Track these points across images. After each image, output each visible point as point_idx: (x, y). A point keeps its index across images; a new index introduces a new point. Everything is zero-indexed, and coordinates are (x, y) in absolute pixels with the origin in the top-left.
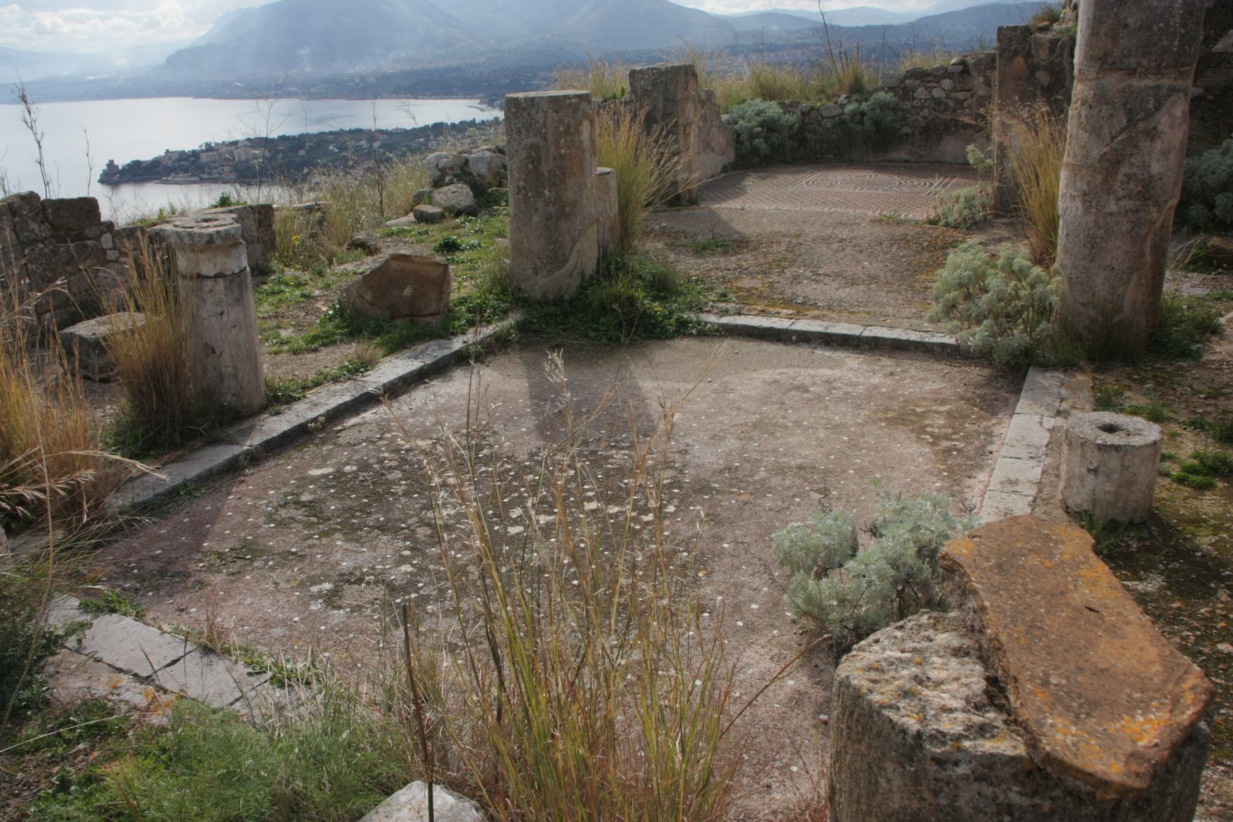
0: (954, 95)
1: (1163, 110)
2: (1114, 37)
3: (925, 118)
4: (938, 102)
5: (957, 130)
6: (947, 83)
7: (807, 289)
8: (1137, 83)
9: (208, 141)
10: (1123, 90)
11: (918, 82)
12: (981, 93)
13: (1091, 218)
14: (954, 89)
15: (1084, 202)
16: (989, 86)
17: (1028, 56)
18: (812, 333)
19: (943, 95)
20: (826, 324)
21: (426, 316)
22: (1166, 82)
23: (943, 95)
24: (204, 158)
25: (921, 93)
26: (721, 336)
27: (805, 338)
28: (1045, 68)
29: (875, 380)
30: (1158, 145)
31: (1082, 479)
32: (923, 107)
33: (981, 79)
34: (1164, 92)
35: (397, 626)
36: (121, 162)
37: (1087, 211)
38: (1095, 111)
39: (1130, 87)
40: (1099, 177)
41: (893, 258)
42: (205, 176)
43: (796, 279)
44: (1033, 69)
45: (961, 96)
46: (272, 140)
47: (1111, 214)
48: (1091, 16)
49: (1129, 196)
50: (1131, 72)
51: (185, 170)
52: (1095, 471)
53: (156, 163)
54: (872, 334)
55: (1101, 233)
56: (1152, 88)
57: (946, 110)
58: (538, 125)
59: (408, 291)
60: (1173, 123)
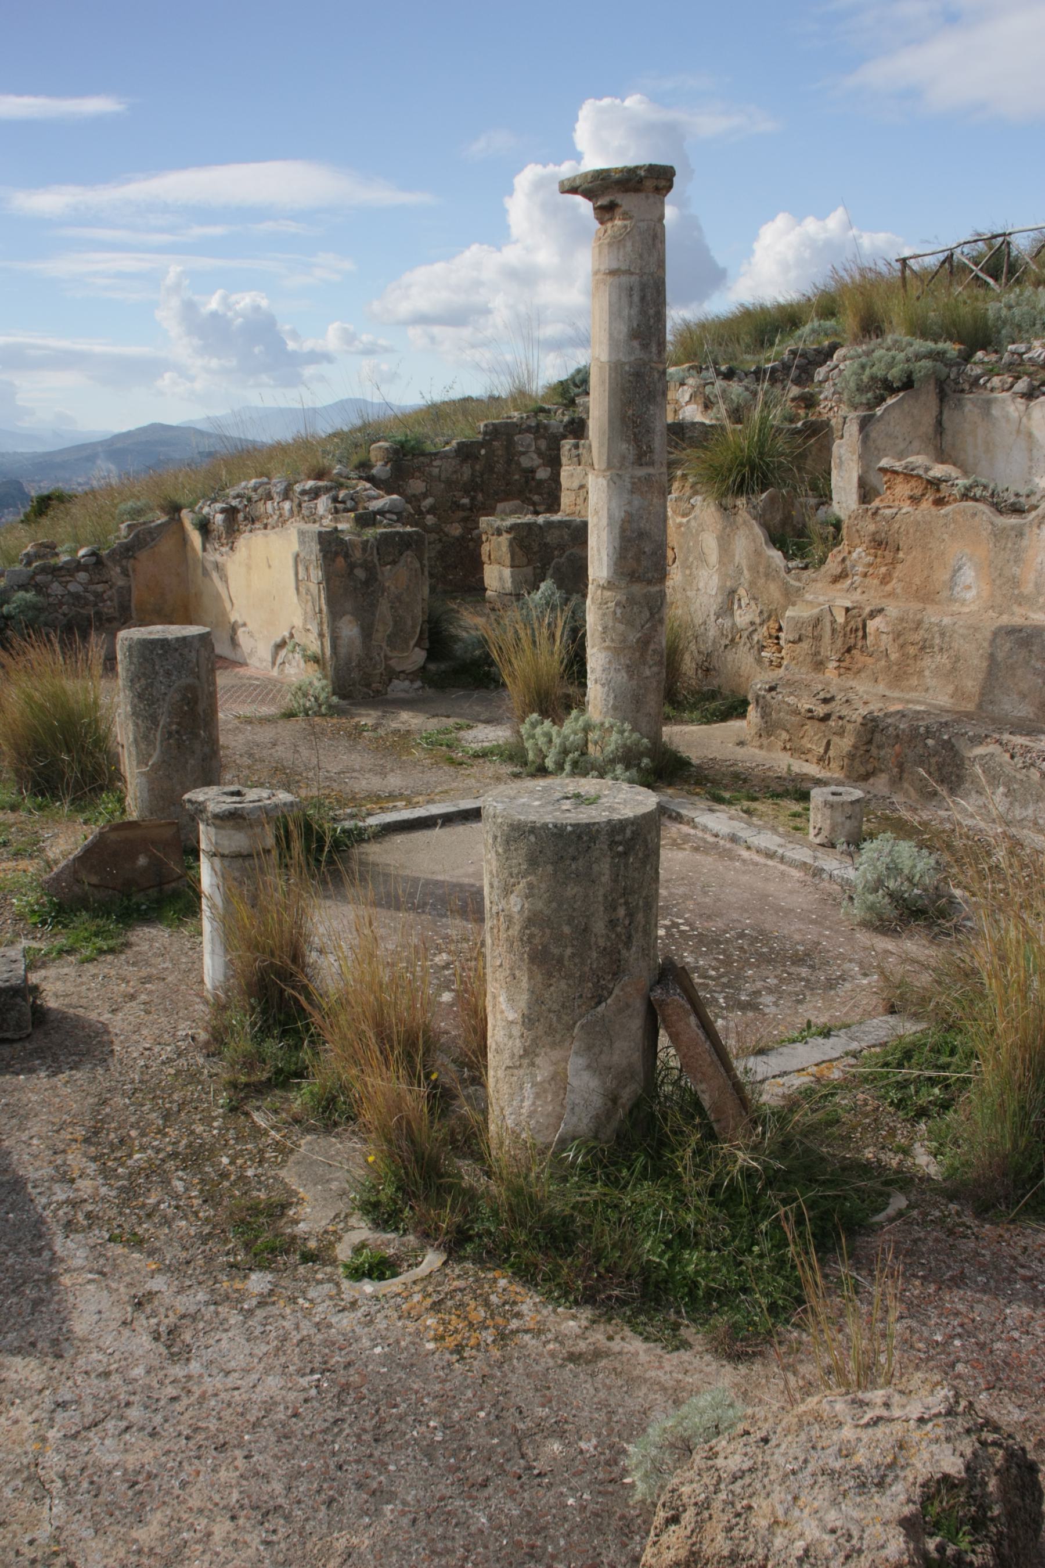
0: (92, 587)
2: (638, 560)
3: (65, 615)
4: (76, 596)
5: (101, 625)
6: (82, 576)
11: (50, 577)
12: (120, 583)
13: (635, 682)
14: (91, 582)
15: (628, 672)
16: (128, 576)
17: (347, 556)
18: (453, 813)
19: (81, 589)
21: (168, 882)
23: (81, 589)
25: (56, 588)
26: (384, 835)
27: (448, 819)
28: (361, 566)
31: (843, 824)
32: (61, 604)
33: (118, 570)
37: (631, 678)
40: (638, 654)
44: (352, 566)
45: (100, 588)
48: (617, 545)
49: (655, 664)
52: (849, 818)
54: (427, 814)
55: (642, 691)
57: (86, 604)
58: (191, 665)
59: (142, 861)
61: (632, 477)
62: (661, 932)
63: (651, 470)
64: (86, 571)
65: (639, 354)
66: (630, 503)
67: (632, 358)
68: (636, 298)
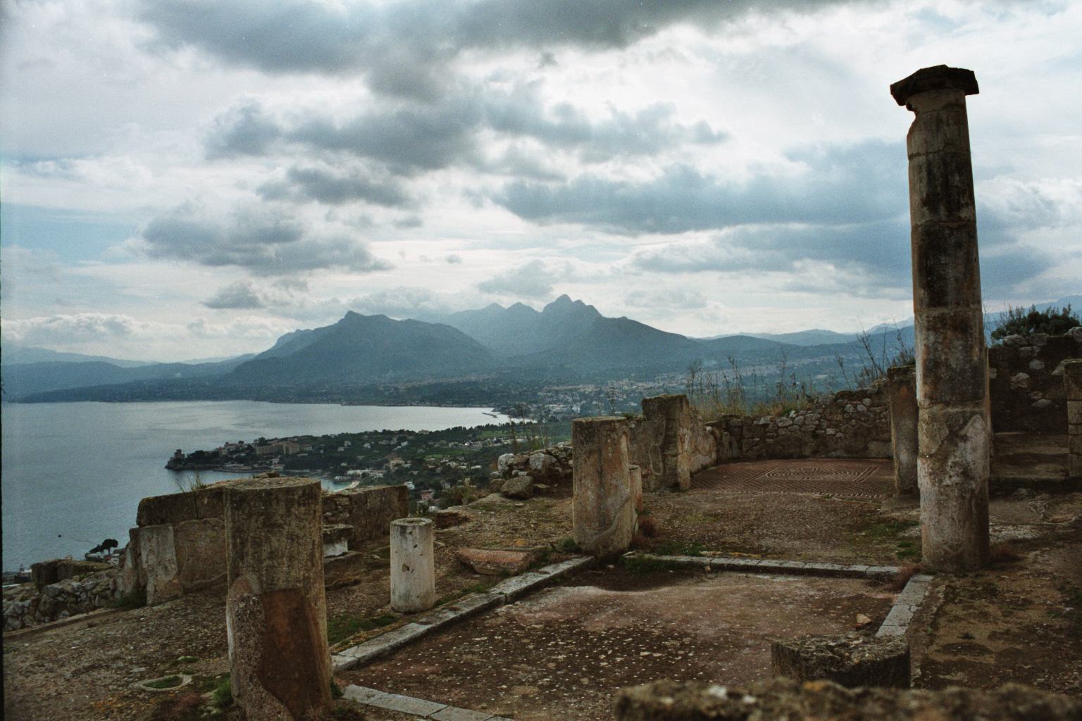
0: (873, 409)
1: (969, 424)
3: (853, 426)
7: (767, 542)
8: (951, 410)
9: (242, 439)
10: (945, 414)
13: (936, 488)
14: (873, 405)
20: (781, 561)
22: (968, 409)
24: (258, 451)
25: (849, 408)
29: (811, 593)
30: (969, 445)
32: (851, 418)
34: (968, 414)
35: (517, 674)
36: (188, 450)
37: (933, 484)
38: (930, 426)
39: (948, 412)
41: (826, 522)
42: (256, 466)
43: (760, 537)
45: (878, 409)
46: (316, 438)
47: (948, 486)
50: (947, 404)
51: (240, 460)
53: (216, 454)
56: (961, 413)
60: (978, 431)
61: (928, 317)
62: (668, 701)
63: (945, 310)
64: (869, 398)
65: (928, 217)
66: (927, 338)
67: (924, 221)
68: (924, 174)
